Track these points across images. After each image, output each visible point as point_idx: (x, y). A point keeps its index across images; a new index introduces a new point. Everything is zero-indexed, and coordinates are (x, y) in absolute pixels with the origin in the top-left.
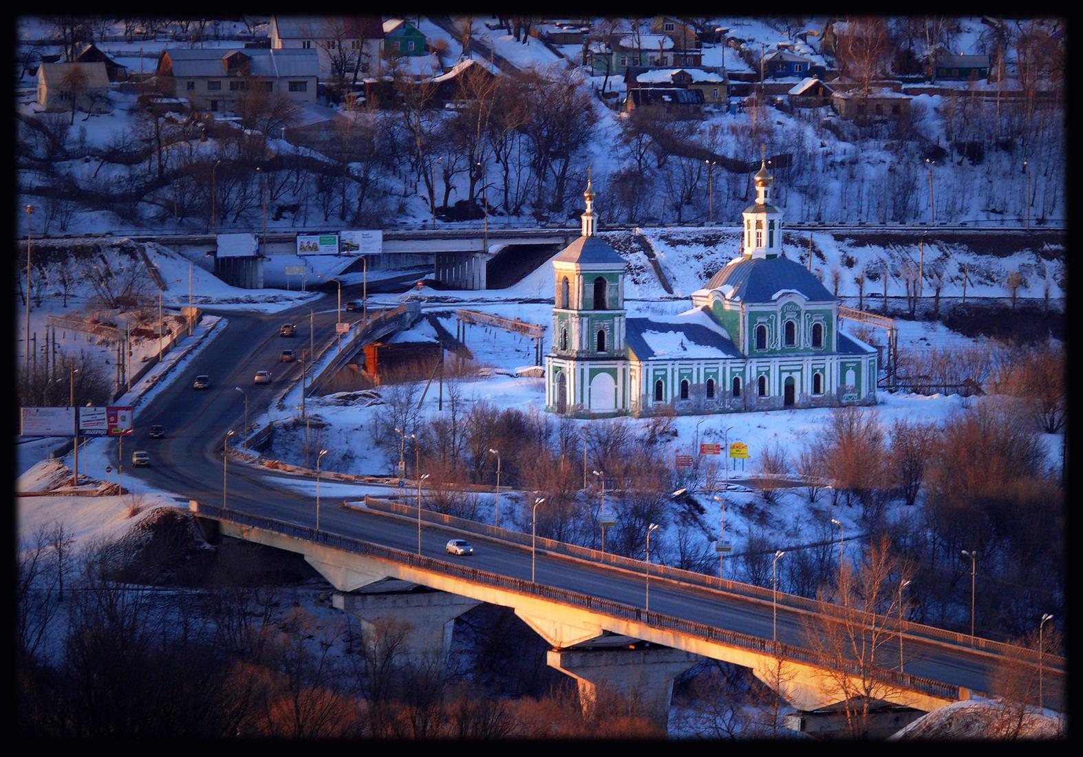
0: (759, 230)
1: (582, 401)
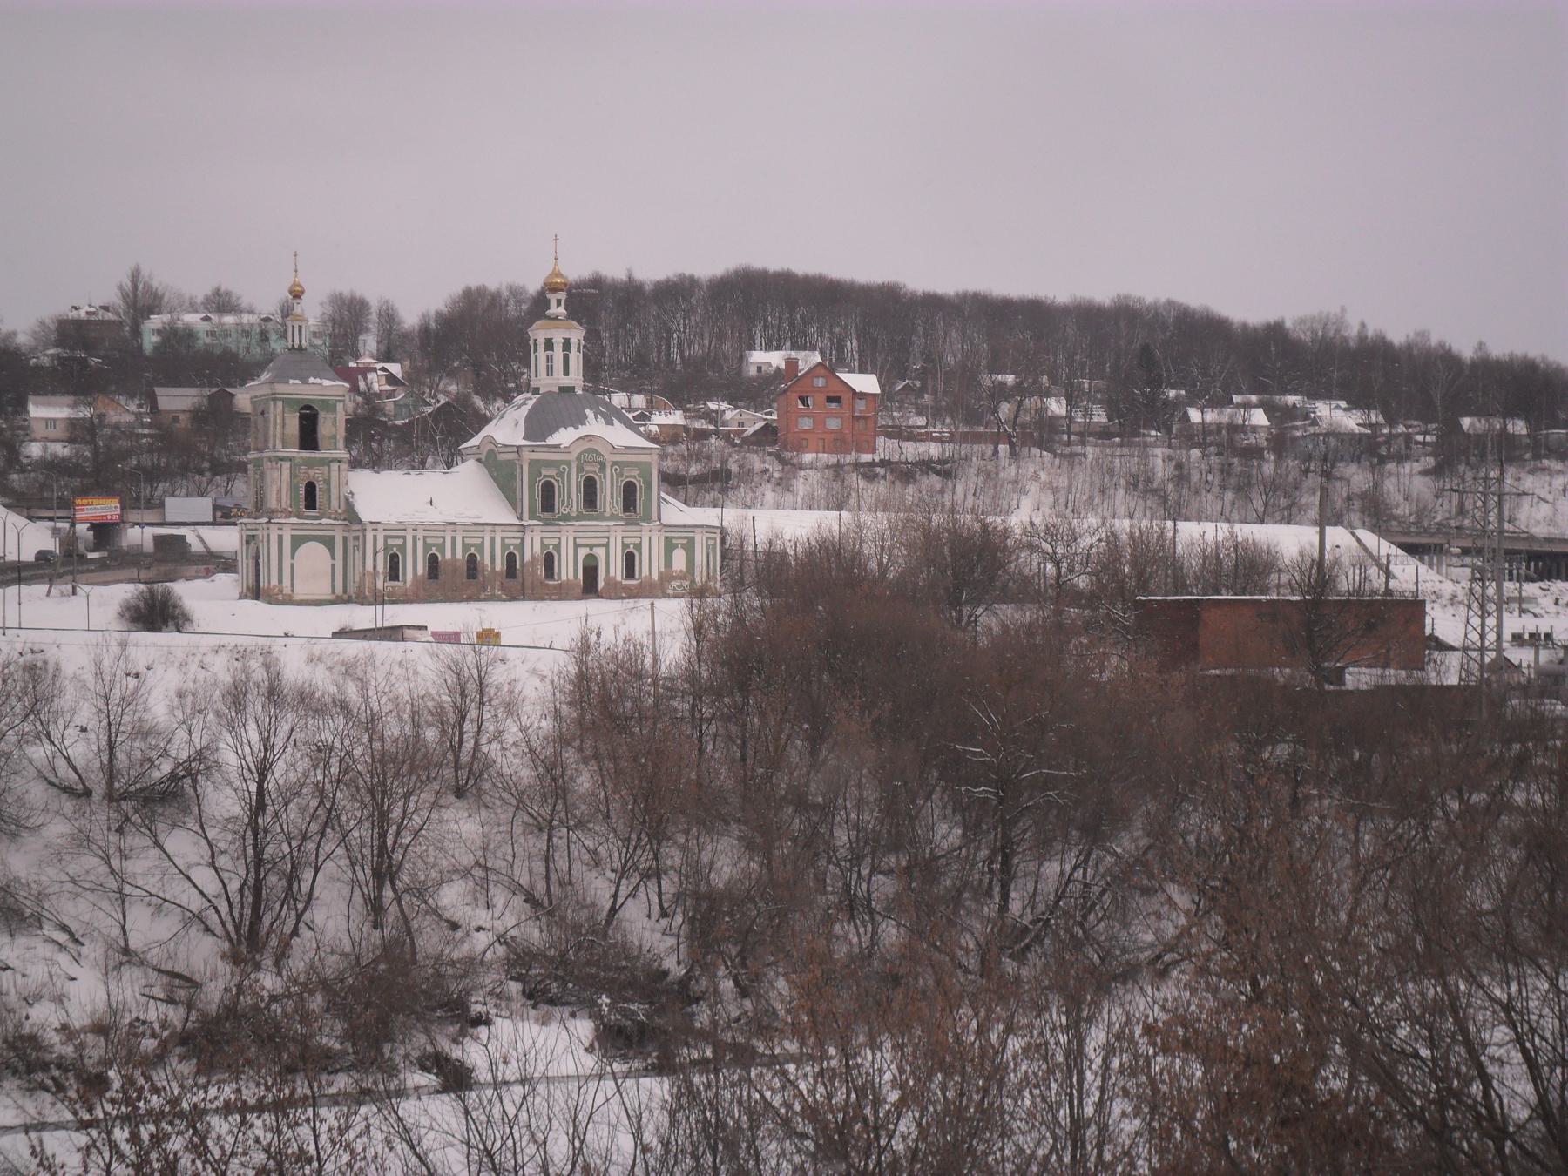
1: (280, 581)
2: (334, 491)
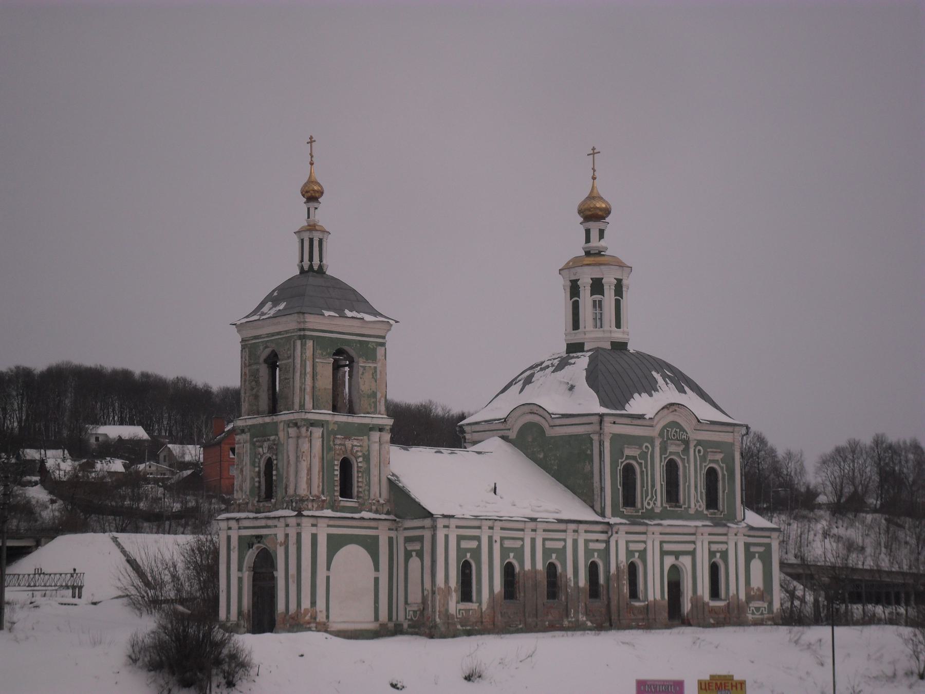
0: (597, 297)
1: (313, 603)
2: (374, 471)
